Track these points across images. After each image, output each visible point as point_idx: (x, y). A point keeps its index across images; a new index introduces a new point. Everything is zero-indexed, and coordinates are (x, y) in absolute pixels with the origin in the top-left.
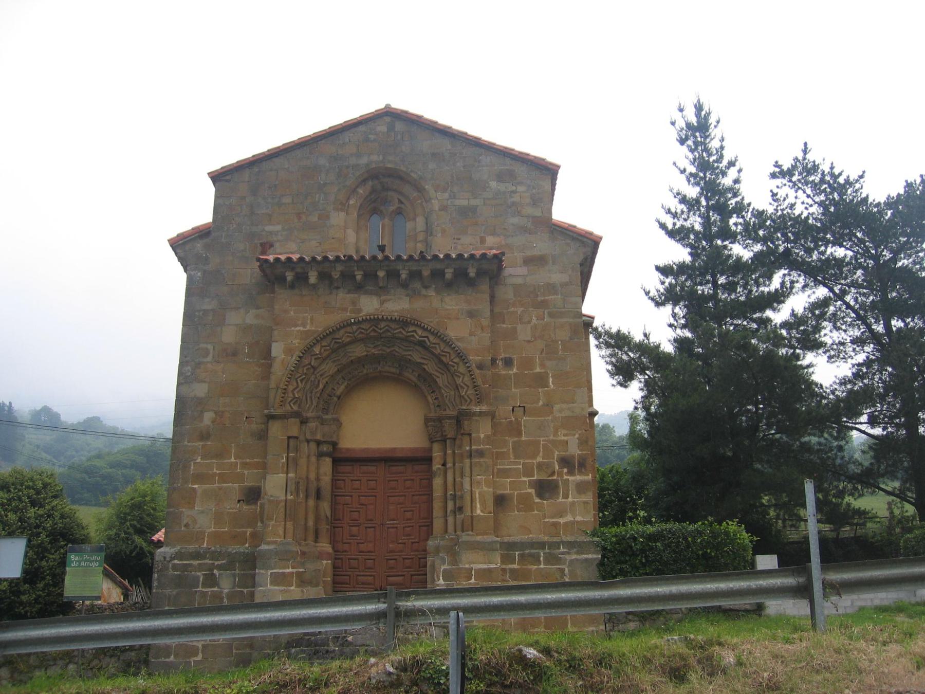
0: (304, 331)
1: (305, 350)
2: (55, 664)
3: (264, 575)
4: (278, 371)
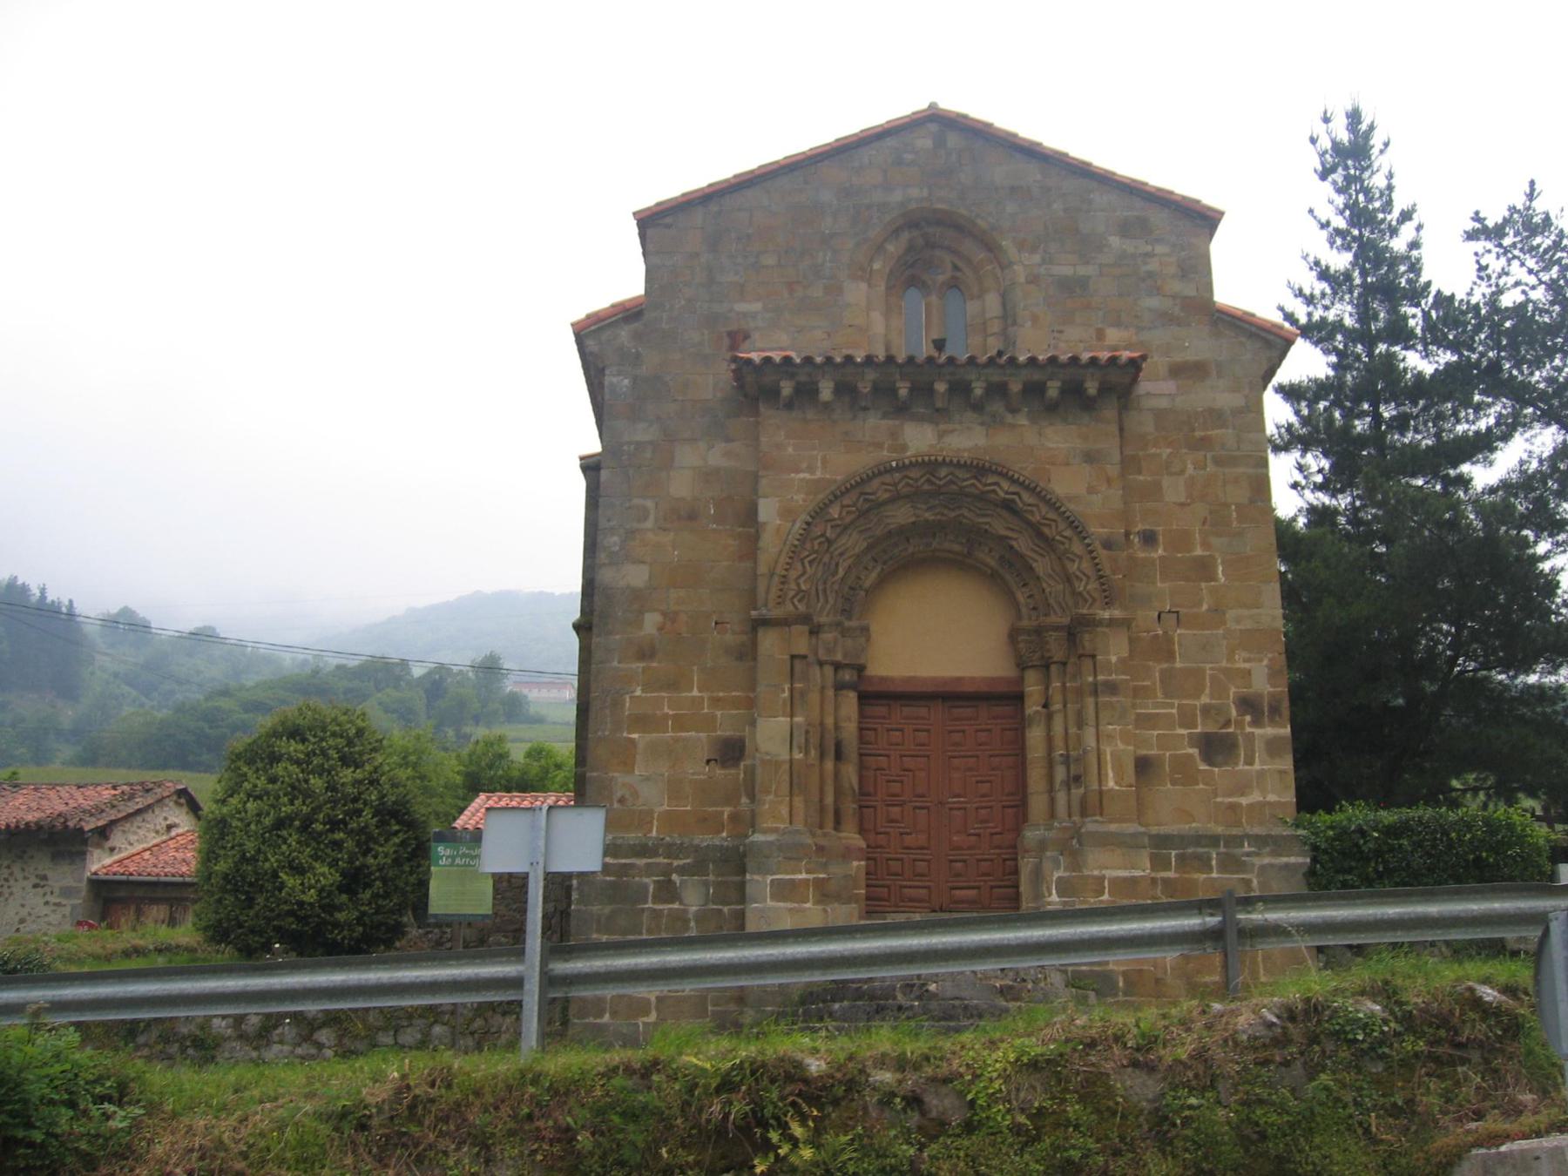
2: (411, 1025)
3: (760, 883)
4: (771, 546)
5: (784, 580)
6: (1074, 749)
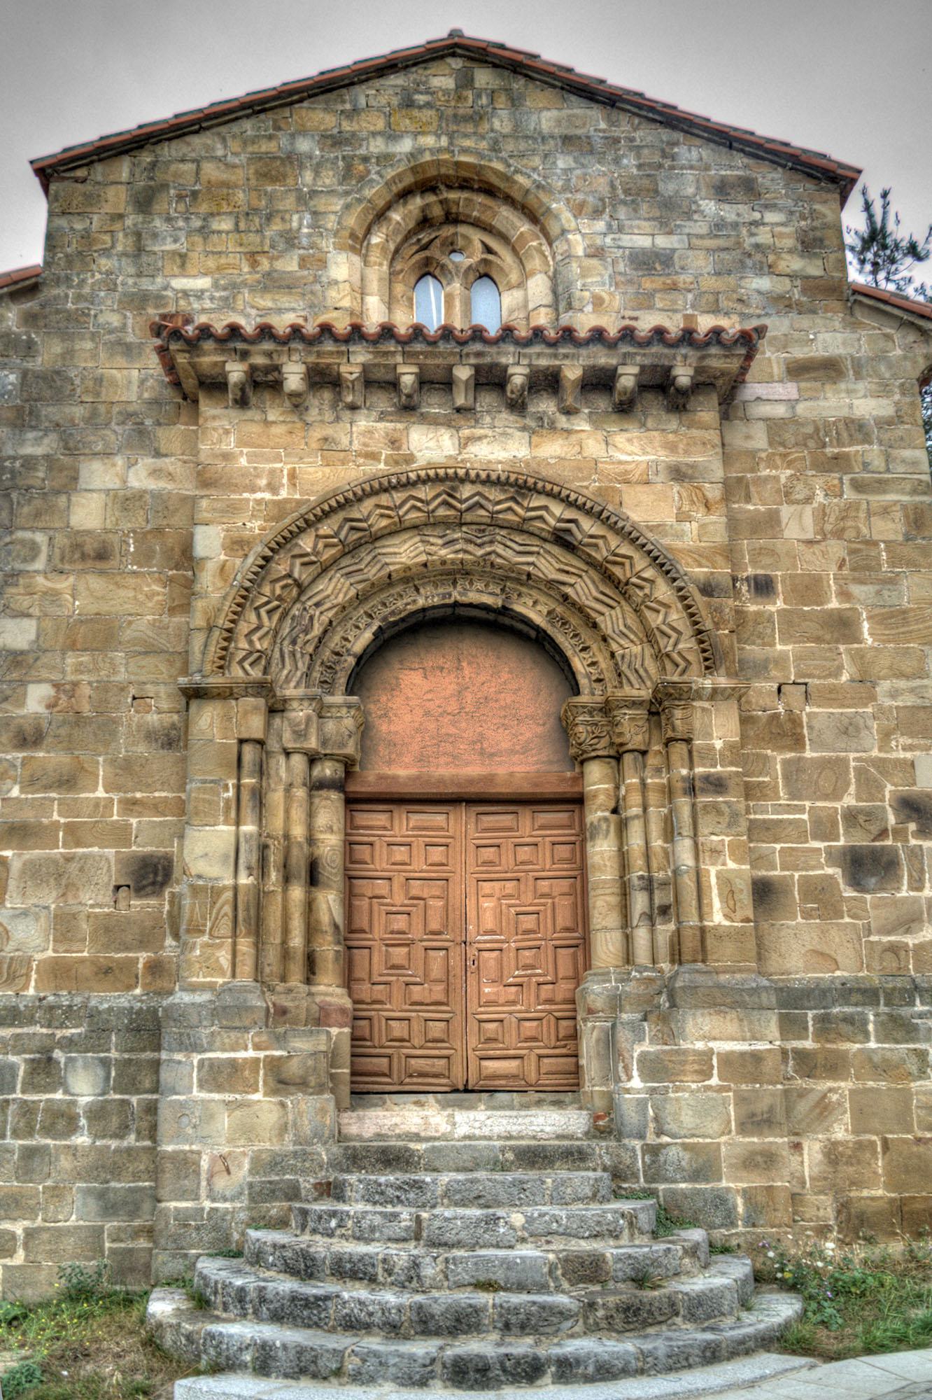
0: (274, 502)
1: (278, 543)
5: (230, 635)
6: (659, 869)
